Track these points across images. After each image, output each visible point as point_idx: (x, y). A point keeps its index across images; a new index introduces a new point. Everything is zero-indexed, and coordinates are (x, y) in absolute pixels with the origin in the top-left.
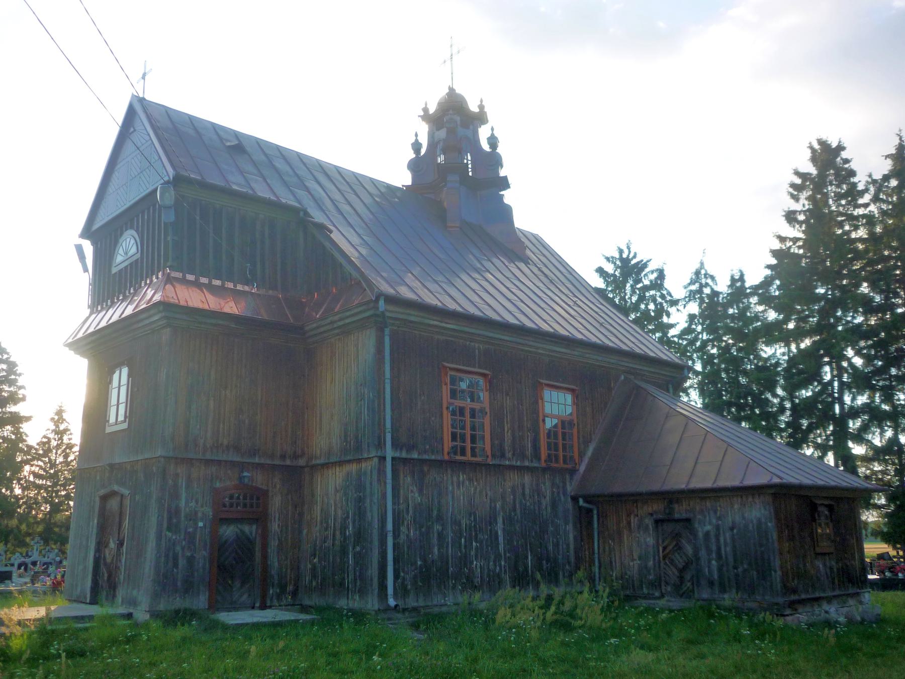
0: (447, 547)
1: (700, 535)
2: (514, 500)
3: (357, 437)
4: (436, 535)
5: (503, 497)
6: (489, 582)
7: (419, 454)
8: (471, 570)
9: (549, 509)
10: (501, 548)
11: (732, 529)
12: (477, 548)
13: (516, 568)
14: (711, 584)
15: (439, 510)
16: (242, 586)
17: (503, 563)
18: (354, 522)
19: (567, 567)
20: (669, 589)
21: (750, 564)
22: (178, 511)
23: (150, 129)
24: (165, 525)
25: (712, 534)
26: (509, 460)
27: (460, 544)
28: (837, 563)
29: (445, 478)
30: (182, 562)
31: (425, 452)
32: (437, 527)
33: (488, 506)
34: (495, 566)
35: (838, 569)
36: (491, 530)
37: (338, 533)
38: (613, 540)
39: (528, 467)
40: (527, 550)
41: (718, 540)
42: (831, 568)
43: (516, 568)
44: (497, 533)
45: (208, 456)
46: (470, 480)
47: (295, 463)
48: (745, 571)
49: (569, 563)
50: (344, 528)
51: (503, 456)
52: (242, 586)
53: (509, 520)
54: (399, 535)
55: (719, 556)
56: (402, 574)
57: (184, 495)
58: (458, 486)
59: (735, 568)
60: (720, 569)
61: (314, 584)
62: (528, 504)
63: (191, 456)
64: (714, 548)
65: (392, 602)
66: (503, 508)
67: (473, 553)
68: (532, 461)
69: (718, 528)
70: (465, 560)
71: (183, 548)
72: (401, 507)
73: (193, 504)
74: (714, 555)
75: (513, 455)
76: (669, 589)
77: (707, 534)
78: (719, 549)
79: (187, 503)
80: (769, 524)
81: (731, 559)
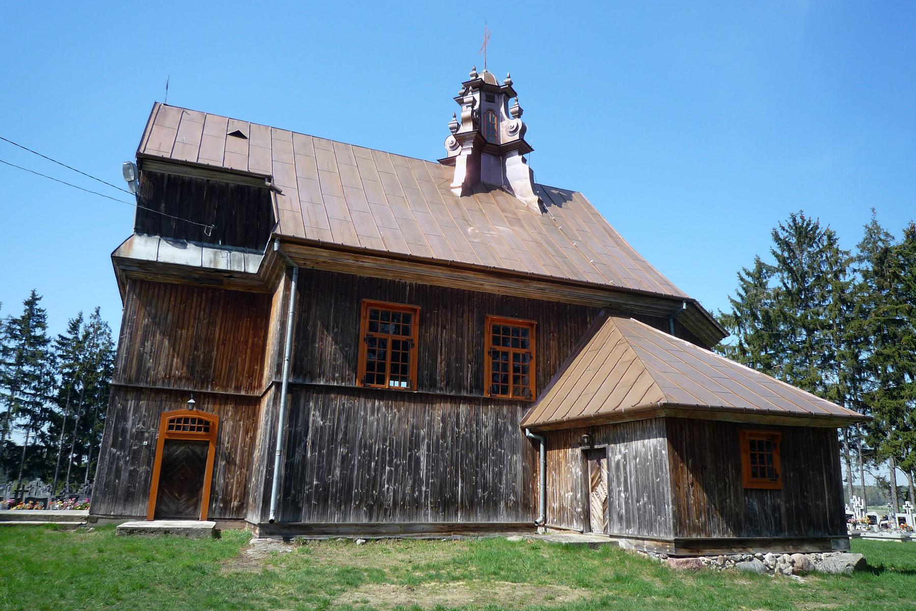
0: (352, 470)
2: (444, 428)
4: (339, 458)
5: (430, 425)
6: (404, 505)
7: (327, 381)
8: (381, 493)
9: (490, 438)
10: (423, 474)
11: (635, 458)
12: (390, 472)
13: (441, 493)
15: (345, 434)
16: (188, 500)
17: (424, 489)
19: (512, 497)
21: (649, 498)
22: (124, 431)
24: (110, 442)
26: (441, 389)
27: (370, 467)
28: (786, 502)
29: (357, 404)
30: (125, 475)
31: (334, 379)
32: (342, 450)
33: (408, 433)
34: (413, 492)
35: (787, 509)
36: (410, 456)
39: (465, 397)
40: (457, 478)
41: (625, 469)
42: (776, 509)
43: (441, 493)
44: (418, 459)
45: (159, 386)
46: (387, 407)
47: (251, 394)
48: (645, 504)
49: (515, 494)
51: (433, 385)
52: (188, 500)
53: (435, 448)
54: (293, 455)
56: (293, 492)
57: (131, 418)
58: (373, 413)
59: (638, 501)
62: (463, 432)
63: (142, 385)
64: (622, 479)
65: (272, 517)
66: (429, 434)
67: (385, 477)
68: (471, 392)
69: (625, 457)
70: (373, 483)
71: (126, 463)
72: (299, 429)
73: (140, 425)
74: (622, 488)
75: (447, 384)
79: (133, 424)
80: (663, 452)
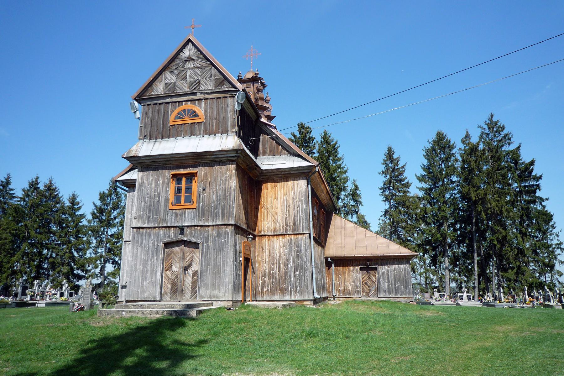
1: (381, 273)
3: (294, 224)
11: (394, 271)
14: (385, 291)
18: (294, 261)
20: (364, 294)
21: (400, 284)
23: (438, 132)
25: (386, 273)
37: (282, 266)
38: (341, 275)
48: (399, 286)
50: (286, 264)
55: (388, 281)
60: (388, 286)
61: (265, 290)
76: (364, 294)
77: (383, 273)
78: (388, 278)
81: (393, 283)
